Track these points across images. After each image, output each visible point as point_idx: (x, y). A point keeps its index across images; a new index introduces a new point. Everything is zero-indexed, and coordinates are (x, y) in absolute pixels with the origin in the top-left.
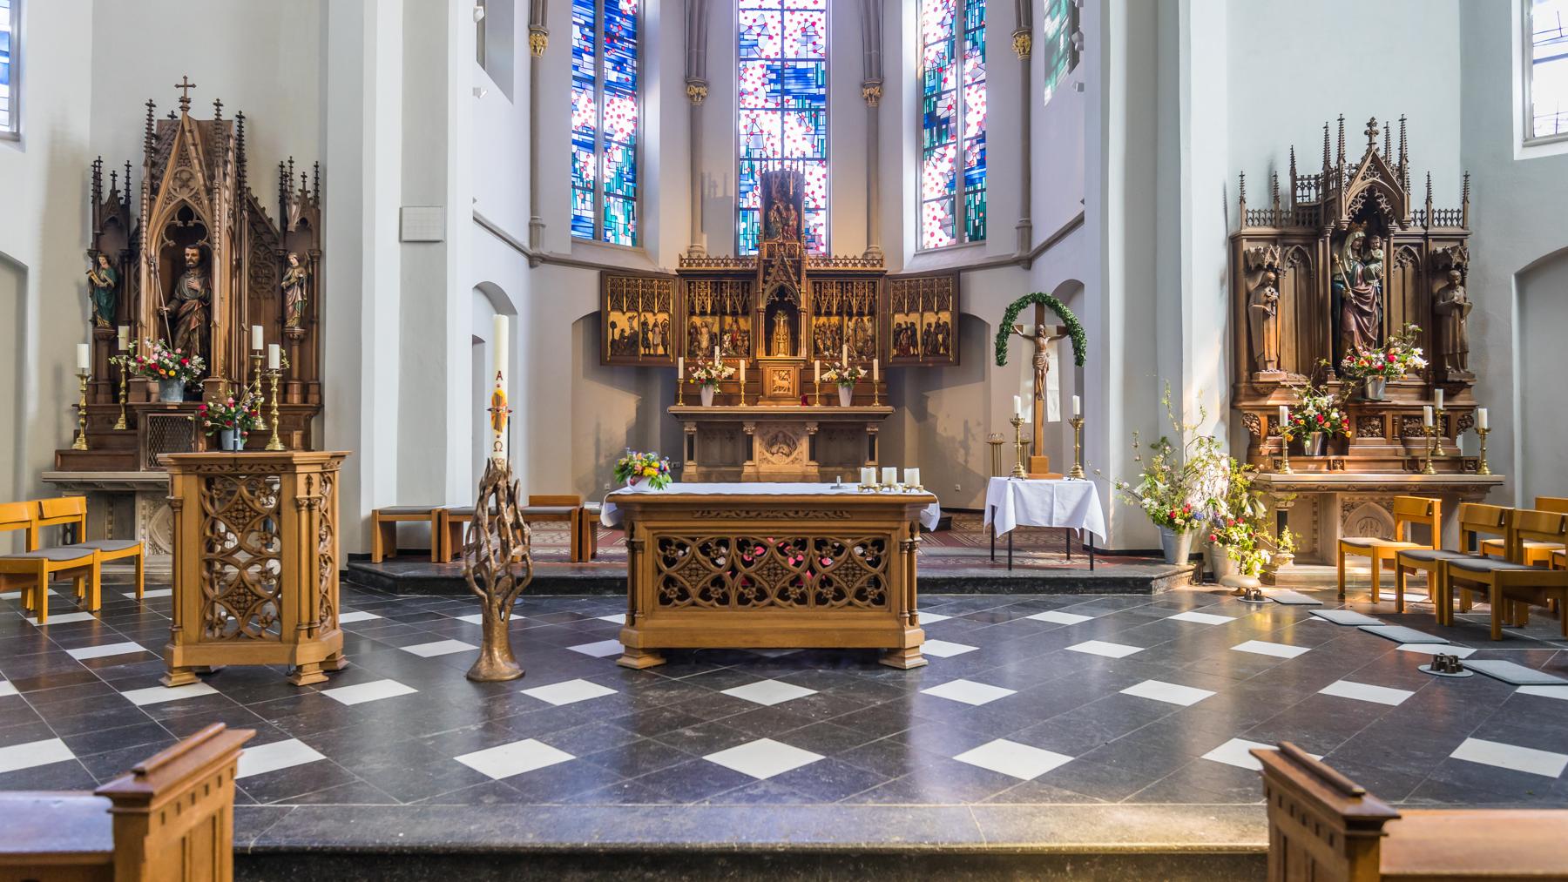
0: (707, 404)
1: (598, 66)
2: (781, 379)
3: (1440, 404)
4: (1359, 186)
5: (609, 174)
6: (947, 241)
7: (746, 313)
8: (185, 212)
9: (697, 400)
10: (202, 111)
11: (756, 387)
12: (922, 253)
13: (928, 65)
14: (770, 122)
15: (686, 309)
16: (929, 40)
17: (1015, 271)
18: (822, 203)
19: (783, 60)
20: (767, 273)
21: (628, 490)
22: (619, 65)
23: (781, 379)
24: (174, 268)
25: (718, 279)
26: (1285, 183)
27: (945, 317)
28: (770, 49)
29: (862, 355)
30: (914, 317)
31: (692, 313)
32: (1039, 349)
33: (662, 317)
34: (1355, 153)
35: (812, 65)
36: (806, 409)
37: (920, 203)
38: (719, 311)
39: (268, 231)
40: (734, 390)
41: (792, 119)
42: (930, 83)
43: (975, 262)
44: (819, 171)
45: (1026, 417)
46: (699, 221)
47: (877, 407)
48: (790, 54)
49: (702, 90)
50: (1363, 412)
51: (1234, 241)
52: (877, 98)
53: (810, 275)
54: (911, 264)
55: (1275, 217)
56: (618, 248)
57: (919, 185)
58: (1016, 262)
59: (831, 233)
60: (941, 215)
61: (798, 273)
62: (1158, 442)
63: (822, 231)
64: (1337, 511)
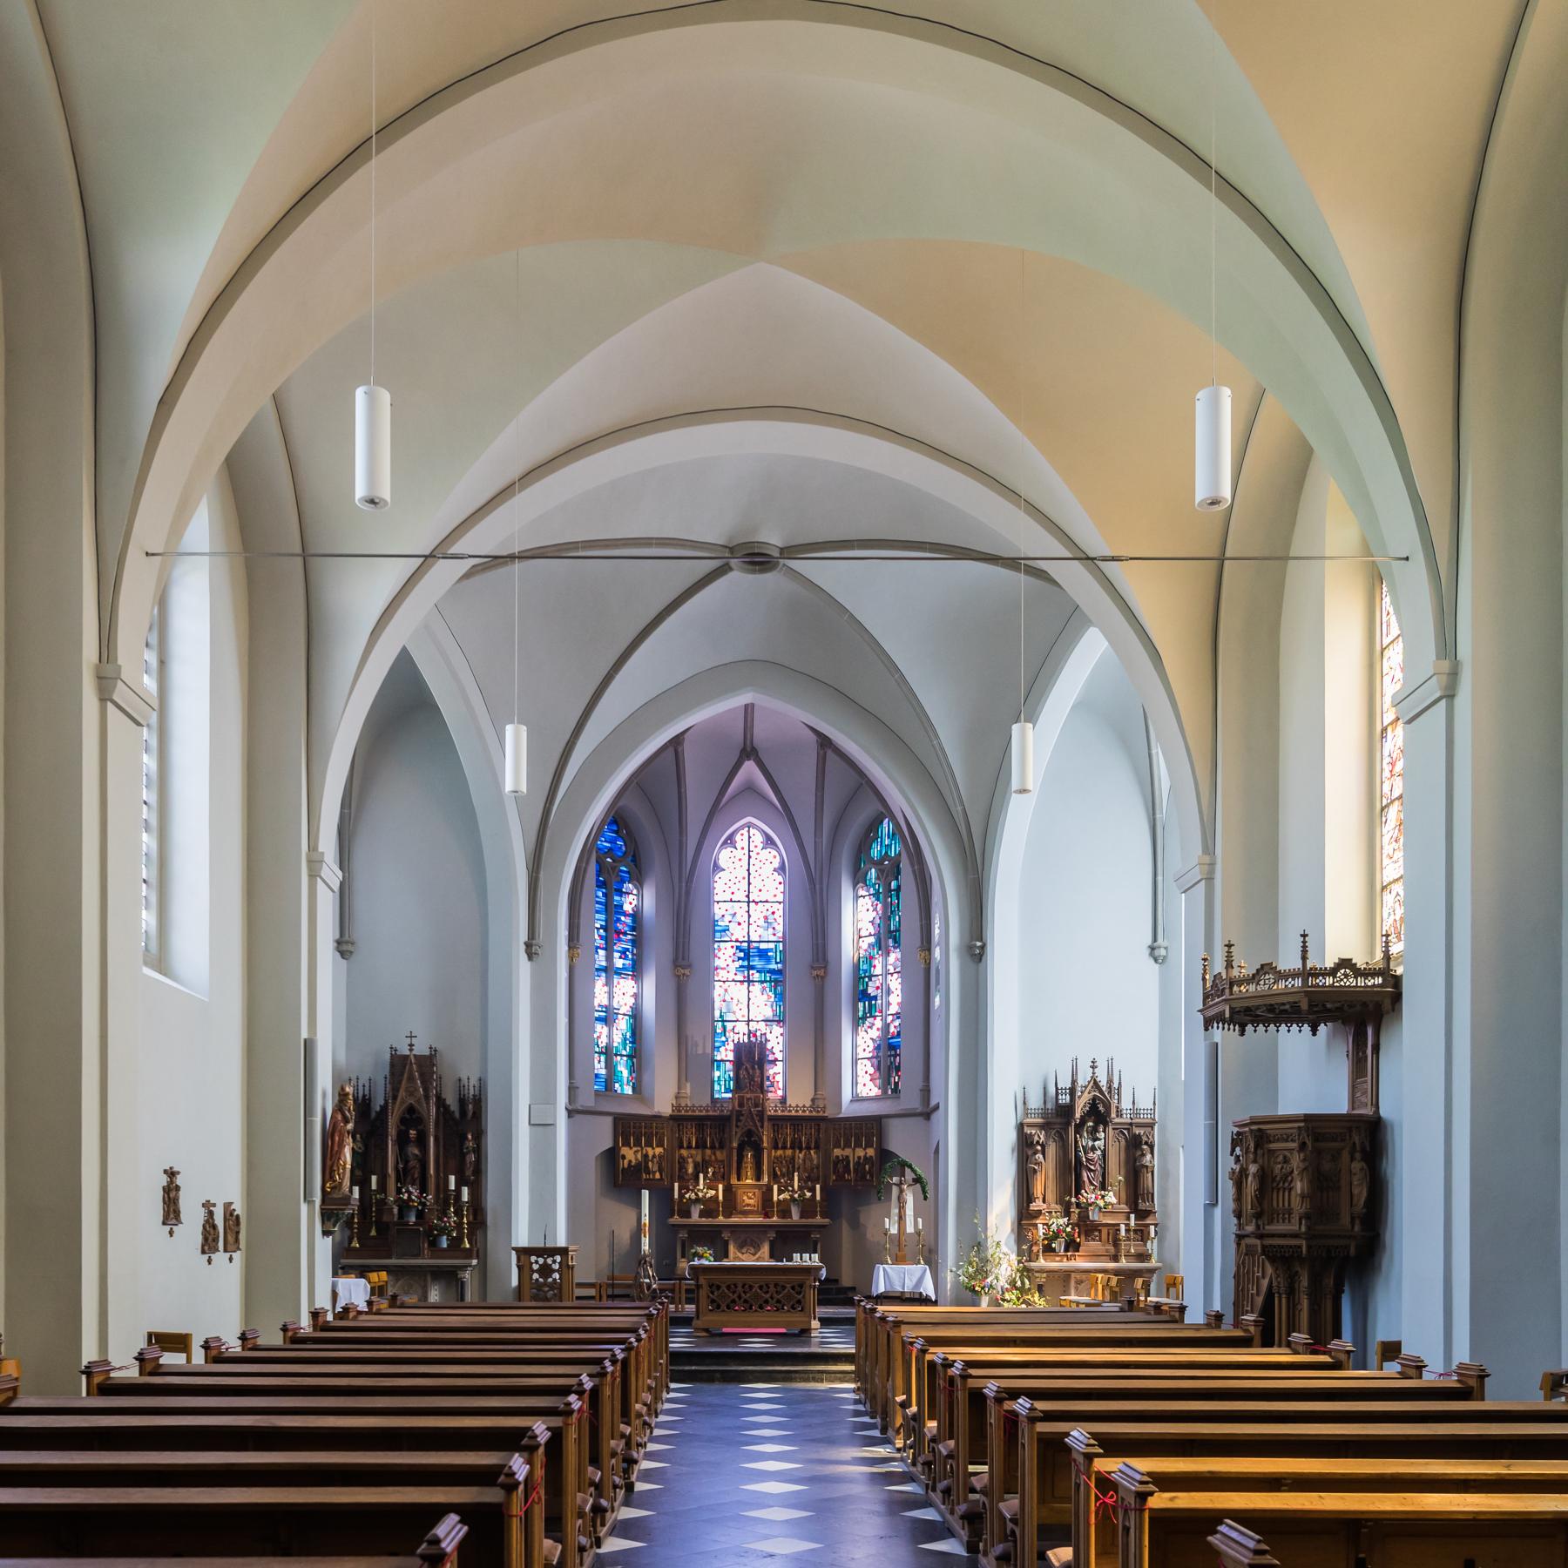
0: (695, 1217)
1: (609, 958)
2: (749, 1199)
3: (1132, 1223)
4: (1086, 1097)
5: (617, 1039)
6: (875, 1091)
7: (721, 1147)
8: (411, 1109)
9: (688, 1215)
10: (421, 1049)
11: (731, 1204)
12: (857, 1099)
13: (862, 953)
14: (739, 991)
15: (676, 1144)
16: (863, 933)
17: (920, 1119)
18: (779, 1056)
19: (749, 942)
20: (738, 1120)
21: (696, 1262)
22: (624, 953)
23: (749, 1199)
24: (402, 1141)
25: (700, 1122)
26: (1052, 1090)
27: (871, 1152)
28: (739, 933)
29: (808, 1182)
30: (848, 1152)
31: (681, 1147)
32: (901, 1191)
33: (659, 1150)
34: (1084, 1078)
35: (772, 946)
36: (768, 1221)
37: (855, 1061)
38: (701, 1145)
39: (453, 1119)
40: (713, 1206)
41: (756, 988)
42: (863, 967)
43: (893, 1112)
44: (777, 1030)
45: (894, 1230)
46: (684, 1073)
47: (818, 1220)
48: (754, 937)
49: (687, 972)
50: (1088, 1228)
51: (1020, 1127)
52: (823, 978)
53: (771, 1118)
54: (847, 1108)
55: (1044, 1113)
56: (623, 1096)
57: (855, 1046)
58: (920, 1114)
59: (784, 1085)
60: (871, 1070)
61: (762, 1121)
62: (975, 1244)
63: (779, 1078)
64: (1073, 1284)
